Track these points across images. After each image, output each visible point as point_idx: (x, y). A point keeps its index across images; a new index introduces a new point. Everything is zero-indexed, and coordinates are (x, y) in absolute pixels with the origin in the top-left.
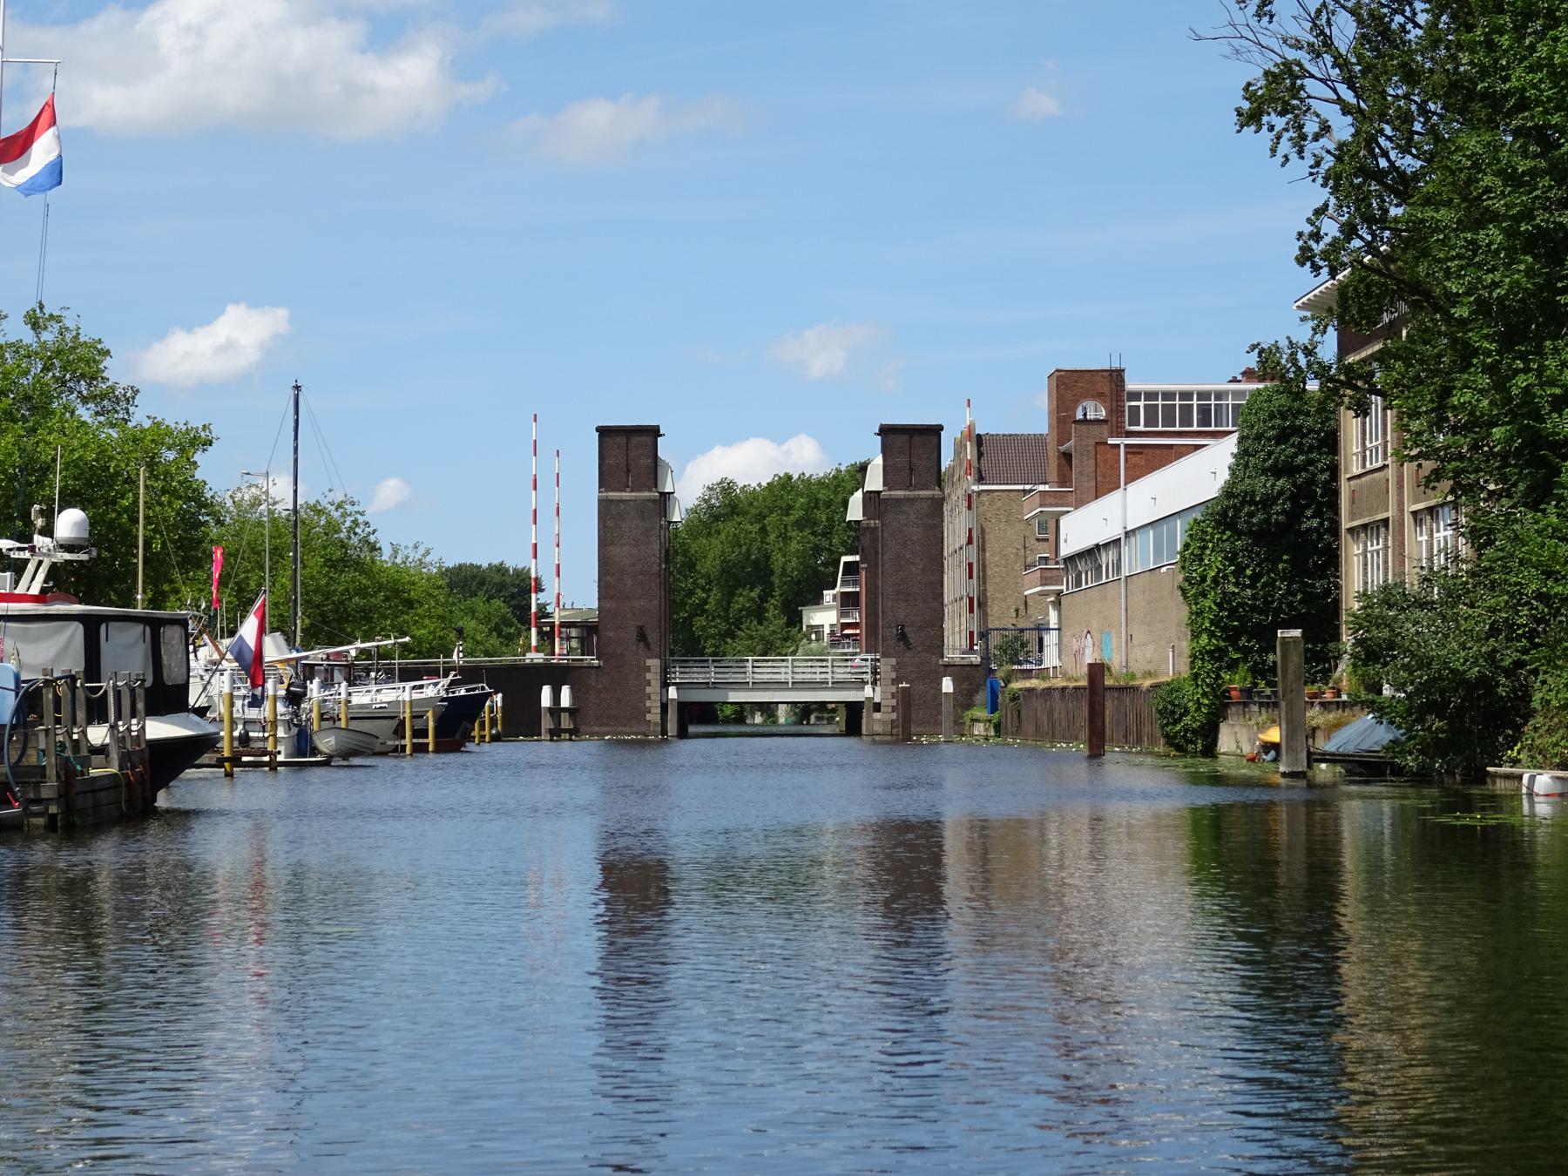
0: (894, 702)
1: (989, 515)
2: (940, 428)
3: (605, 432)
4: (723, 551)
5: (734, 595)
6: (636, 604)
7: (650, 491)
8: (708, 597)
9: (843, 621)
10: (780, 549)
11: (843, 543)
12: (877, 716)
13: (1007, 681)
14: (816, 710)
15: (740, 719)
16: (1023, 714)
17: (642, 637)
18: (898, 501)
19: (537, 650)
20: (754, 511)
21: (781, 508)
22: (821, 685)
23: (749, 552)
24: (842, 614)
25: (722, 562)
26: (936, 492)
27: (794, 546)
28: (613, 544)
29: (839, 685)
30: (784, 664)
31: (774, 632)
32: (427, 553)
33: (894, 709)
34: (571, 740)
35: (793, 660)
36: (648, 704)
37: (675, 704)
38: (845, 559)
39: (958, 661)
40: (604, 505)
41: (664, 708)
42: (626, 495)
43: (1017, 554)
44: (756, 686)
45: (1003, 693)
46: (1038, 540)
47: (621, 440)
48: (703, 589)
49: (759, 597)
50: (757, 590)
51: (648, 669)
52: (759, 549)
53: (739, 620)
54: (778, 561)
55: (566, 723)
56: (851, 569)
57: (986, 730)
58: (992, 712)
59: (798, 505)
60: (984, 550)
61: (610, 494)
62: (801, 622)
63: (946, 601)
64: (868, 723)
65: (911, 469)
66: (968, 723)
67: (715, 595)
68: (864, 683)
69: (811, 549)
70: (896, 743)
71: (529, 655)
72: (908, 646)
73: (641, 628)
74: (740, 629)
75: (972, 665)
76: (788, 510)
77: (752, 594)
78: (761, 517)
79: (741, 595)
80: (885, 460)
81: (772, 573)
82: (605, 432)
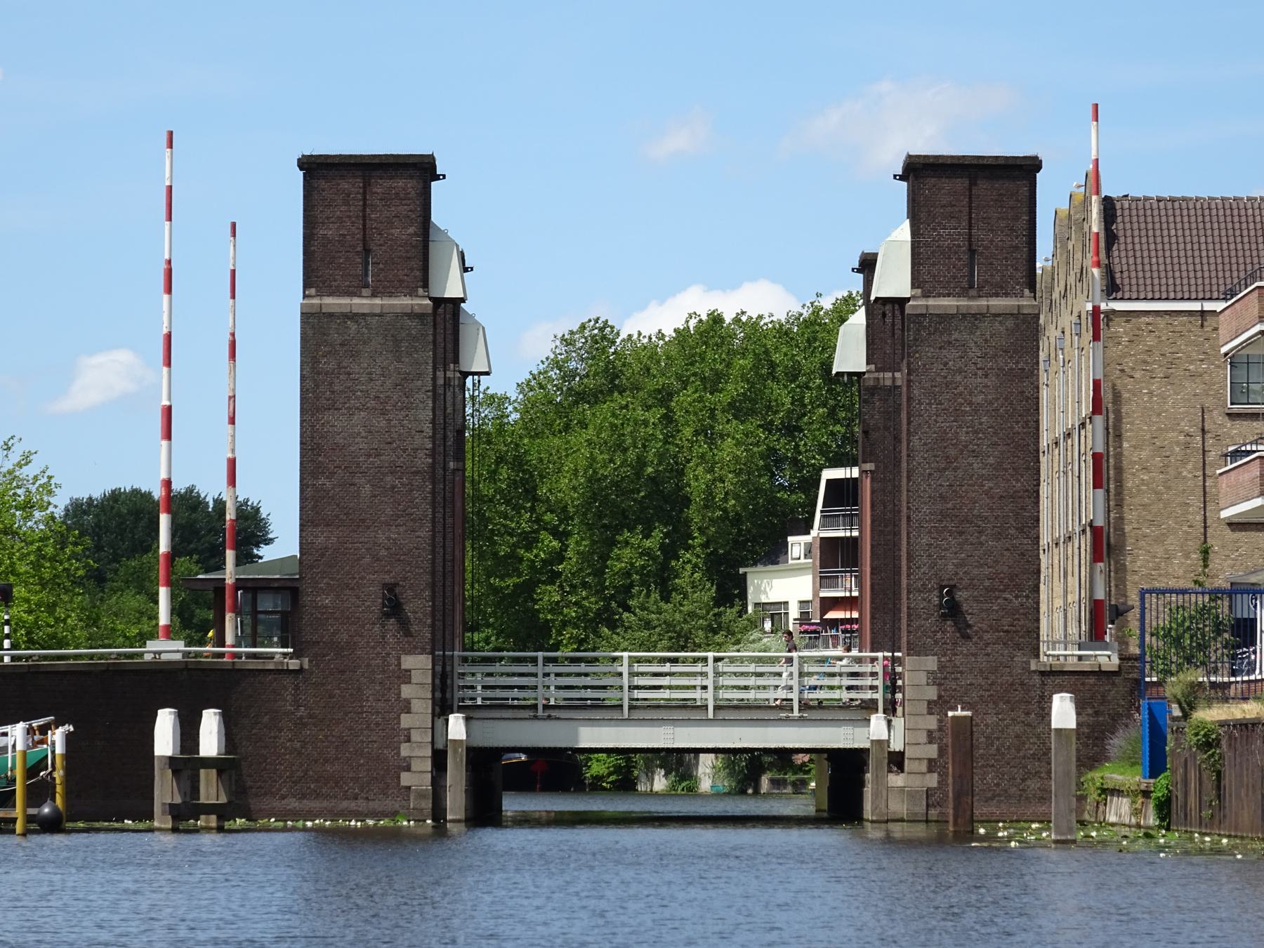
0: (932, 750)
1: (1129, 363)
2: (1027, 169)
3: (314, 167)
4: (593, 459)
5: (612, 543)
6: (381, 538)
7: (412, 293)
8: (565, 548)
9: (826, 593)
10: (702, 457)
11: (823, 449)
12: (896, 780)
13: (1188, 707)
14: (771, 766)
15: (626, 784)
16: (1229, 779)
17: (393, 607)
18: (944, 318)
19: (170, 633)
20: (651, 385)
21: (703, 379)
22: (777, 712)
23: (641, 463)
24: (824, 581)
25: (590, 480)
26: (1026, 302)
27: (728, 450)
28: (333, 407)
29: (814, 710)
30: (699, 668)
31: (692, 615)
32: (26, 460)
33: (932, 765)
34: (220, 829)
35: (717, 660)
36: (405, 750)
37: (462, 751)
38: (829, 474)
39: (1072, 664)
40: (311, 323)
41: (439, 759)
42: (361, 303)
43: (1187, 446)
44: (637, 714)
45: (1179, 731)
46: (1232, 416)
47: (351, 185)
48: (555, 533)
49: (662, 547)
50: (657, 534)
51: (406, 677)
52: (661, 457)
53: (627, 590)
54: (697, 480)
55: (210, 790)
56: (842, 493)
57: (1136, 812)
58: (1154, 773)
59: (734, 372)
60: (1119, 436)
61: (328, 300)
62: (743, 596)
63: (1044, 540)
64: (876, 795)
65: (972, 252)
66: (1093, 796)
67: (576, 545)
68: (870, 706)
69: (762, 456)
70: (939, 841)
71: (152, 646)
72: (964, 631)
73: (391, 588)
74: (628, 609)
75: (1100, 674)
76: (713, 383)
77: (648, 543)
78: (664, 397)
79: (627, 543)
80: (915, 233)
81: (687, 501)
82: (314, 167)
